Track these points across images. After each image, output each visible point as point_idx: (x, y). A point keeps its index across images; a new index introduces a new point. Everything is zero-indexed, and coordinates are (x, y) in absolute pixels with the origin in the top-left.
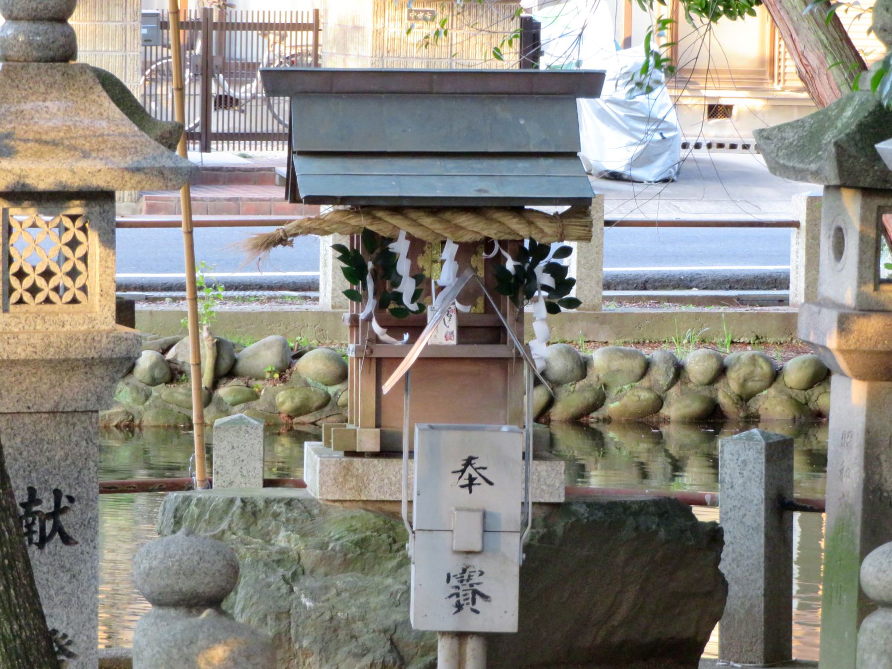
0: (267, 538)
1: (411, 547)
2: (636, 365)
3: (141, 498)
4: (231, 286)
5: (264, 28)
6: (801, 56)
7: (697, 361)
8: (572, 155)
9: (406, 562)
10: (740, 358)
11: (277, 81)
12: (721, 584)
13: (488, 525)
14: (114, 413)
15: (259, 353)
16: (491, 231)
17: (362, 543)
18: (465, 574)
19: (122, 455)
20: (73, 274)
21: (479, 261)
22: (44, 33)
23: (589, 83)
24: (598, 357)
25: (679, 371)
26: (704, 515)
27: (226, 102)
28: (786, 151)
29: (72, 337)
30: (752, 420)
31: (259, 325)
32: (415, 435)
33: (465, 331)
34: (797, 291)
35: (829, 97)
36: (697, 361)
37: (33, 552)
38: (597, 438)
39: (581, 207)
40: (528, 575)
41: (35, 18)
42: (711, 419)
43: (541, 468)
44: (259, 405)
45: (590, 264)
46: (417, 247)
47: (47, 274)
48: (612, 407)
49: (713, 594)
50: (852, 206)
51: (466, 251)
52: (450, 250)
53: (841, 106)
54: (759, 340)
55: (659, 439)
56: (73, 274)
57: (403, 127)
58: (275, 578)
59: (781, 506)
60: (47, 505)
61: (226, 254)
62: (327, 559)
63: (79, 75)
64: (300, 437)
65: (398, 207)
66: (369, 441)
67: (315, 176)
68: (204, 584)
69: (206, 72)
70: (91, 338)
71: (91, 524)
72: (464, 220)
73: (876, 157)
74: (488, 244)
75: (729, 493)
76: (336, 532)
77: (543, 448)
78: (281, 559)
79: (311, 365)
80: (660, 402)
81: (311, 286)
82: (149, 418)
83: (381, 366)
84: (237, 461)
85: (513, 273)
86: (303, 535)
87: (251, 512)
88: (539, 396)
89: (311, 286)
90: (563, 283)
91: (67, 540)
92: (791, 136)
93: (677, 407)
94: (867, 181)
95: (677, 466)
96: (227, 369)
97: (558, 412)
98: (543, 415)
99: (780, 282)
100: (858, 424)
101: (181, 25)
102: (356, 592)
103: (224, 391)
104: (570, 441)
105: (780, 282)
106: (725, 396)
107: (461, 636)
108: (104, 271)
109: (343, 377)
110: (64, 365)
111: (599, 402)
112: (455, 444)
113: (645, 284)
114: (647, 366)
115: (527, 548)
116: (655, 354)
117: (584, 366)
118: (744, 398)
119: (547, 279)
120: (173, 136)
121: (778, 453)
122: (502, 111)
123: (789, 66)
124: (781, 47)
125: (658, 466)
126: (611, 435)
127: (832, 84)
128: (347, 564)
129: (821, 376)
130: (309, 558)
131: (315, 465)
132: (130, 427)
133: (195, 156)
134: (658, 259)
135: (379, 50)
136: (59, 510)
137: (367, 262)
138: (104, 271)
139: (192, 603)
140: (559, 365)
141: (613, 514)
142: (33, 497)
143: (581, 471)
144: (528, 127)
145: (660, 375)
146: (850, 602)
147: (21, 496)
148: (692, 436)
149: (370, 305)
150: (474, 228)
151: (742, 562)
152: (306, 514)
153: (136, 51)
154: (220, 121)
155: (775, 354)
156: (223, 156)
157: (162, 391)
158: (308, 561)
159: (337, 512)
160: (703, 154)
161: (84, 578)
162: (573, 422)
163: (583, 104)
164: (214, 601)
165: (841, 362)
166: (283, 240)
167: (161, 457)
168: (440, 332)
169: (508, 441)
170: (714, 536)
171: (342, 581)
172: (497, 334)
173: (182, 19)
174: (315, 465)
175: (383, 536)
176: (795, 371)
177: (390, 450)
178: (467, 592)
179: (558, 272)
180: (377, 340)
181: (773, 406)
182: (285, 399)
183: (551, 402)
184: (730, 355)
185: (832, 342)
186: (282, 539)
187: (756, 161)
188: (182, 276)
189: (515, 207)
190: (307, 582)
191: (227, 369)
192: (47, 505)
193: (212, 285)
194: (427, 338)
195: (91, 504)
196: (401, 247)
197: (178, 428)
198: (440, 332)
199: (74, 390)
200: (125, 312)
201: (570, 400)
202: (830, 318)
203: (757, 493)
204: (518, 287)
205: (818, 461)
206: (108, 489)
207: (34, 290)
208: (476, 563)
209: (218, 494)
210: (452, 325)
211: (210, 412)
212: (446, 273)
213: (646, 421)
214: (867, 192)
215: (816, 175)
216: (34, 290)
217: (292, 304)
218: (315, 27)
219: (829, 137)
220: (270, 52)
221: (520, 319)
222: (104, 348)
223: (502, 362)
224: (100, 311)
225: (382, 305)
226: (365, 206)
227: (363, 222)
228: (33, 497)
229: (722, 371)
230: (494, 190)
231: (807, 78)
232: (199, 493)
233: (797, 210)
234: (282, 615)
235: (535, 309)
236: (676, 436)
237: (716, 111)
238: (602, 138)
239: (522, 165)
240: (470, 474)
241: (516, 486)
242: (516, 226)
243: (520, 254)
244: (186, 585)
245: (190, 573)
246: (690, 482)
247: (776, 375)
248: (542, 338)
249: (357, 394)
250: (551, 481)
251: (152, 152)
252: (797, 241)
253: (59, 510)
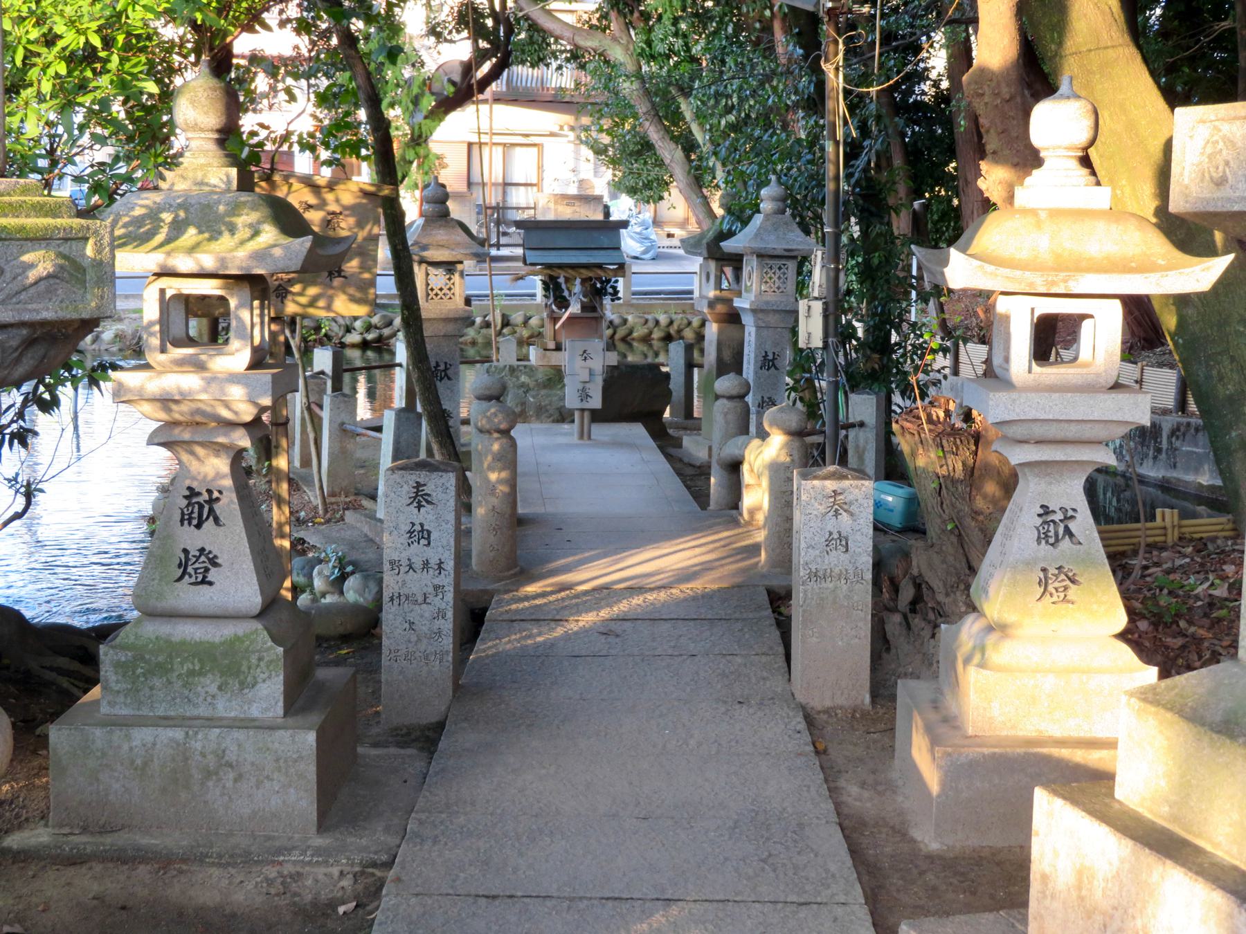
0: (518, 378)
1: (566, 381)
2: (643, 321)
3: (478, 365)
4: (507, 295)
5: (518, 208)
6: (697, 216)
7: (663, 319)
8: (618, 249)
9: (564, 386)
10: (678, 318)
11: (519, 224)
12: (670, 392)
13: (591, 373)
14: (468, 338)
15: (517, 318)
16: (590, 274)
17: (549, 380)
18: (584, 389)
19: (471, 352)
20: (450, 289)
21: (587, 285)
22: (438, 207)
23: (624, 224)
24: (630, 318)
25: (657, 322)
26: (664, 369)
27: (505, 234)
28: (691, 245)
29: (450, 310)
30: (682, 338)
31: (516, 308)
32: (567, 343)
33: (584, 308)
34: (696, 294)
35: (705, 228)
36: (663, 319)
37: (438, 383)
38: (630, 345)
39: (621, 268)
40: (606, 390)
41: (436, 202)
42: (668, 338)
43: (609, 354)
44: (517, 335)
45: (627, 286)
46: (567, 280)
47: (441, 289)
48: (635, 335)
49: (666, 397)
50: (712, 265)
51: (584, 281)
52: (578, 281)
53: (709, 231)
54: (684, 312)
55: (651, 346)
56: (450, 289)
57: (561, 240)
58: (521, 391)
59: (690, 366)
60: (442, 367)
61: (503, 285)
62: (538, 385)
63: (61, 44)
64: (529, 344)
65: (561, 266)
66: (552, 345)
67: (533, 256)
68: (494, 392)
69: (498, 223)
70: (457, 310)
71: (457, 373)
72: (583, 271)
73: (720, 248)
74: (591, 279)
75: (672, 362)
76: (540, 376)
77: (611, 346)
78: (523, 385)
79: (534, 322)
80: (651, 333)
81: (534, 295)
82: (480, 340)
83: (555, 320)
84: (507, 353)
85: (598, 289)
86: (530, 377)
87: (513, 370)
88: (609, 332)
89: (534, 295)
90: (616, 292)
91: (449, 379)
92: (692, 241)
93: (657, 334)
94: (718, 256)
95: (657, 355)
96: (506, 323)
97: (617, 336)
98: (612, 337)
99: (691, 292)
100: (715, 337)
101: (487, 208)
102: (548, 396)
103: (505, 331)
104: (621, 346)
105: (691, 292)
106: (672, 331)
107: (583, 410)
108: (460, 287)
109: (543, 326)
110: (447, 320)
111: (631, 333)
112: (580, 346)
113: (646, 293)
114: (646, 321)
115: (605, 381)
116: (649, 317)
117: (625, 321)
118: (679, 331)
119: (610, 290)
120: (482, 243)
121: (689, 349)
122: (595, 234)
123: (693, 220)
124: (691, 214)
125: (650, 354)
126: (635, 344)
127: (707, 224)
128: (545, 387)
129: (703, 324)
130: (532, 384)
131: (533, 353)
132: (474, 343)
133: (494, 252)
134: (650, 285)
135: (556, 214)
136: (446, 369)
137: (552, 286)
138: (460, 287)
139: (489, 398)
140: (617, 321)
141: (634, 368)
142: (438, 365)
143: (625, 356)
144: (605, 241)
145: (651, 324)
146: (712, 397)
147: (433, 364)
148: (660, 344)
149: (552, 300)
150: (586, 273)
151: (677, 384)
152: (531, 370)
153: (474, 216)
154: (503, 240)
155: (689, 317)
156: (504, 252)
157: (484, 331)
158: (531, 386)
159: (541, 369)
160: (666, 250)
161: (455, 395)
162: (619, 340)
163: (623, 231)
164: (498, 398)
165: (709, 317)
166: (522, 278)
167: (484, 353)
168: (575, 308)
169: (597, 345)
170: (667, 375)
171: (543, 392)
172: (594, 309)
173: (801, 345)
174: (533, 353)
175: (556, 377)
176: (696, 322)
177: (558, 348)
178: (585, 395)
179: (614, 288)
180: (553, 311)
181: (689, 334)
182: (525, 333)
183: (614, 333)
184: (674, 317)
185: (706, 310)
186: (523, 378)
187: (681, 252)
188: (488, 292)
189: (600, 266)
190: (532, 393)
191: (506, 323)
192: (442, 367)
193: (501, 295)
194: (570, 310)
195: (457, 367)
196: (561, 280)
197: (488, 344)
198: (575, 308)
199: (450, 328)
200: (468, 301)
201: (621, 332)
202: (705, 303)
203: (682, 362)
204: (600, 293)
205: (702, 351)
206: (462, 363)
207: (437, 295)
208: (588, 385)
209: (501, 364)
210: (579, 306)
211: (501, 339)
212: (577, 288)
213: (646, 339)
214: (717, 260)
215: (700, 254)
216: (437, 295)
217: (528, 301)
218: (534, 208)
219: (705, 241)
220: (520, 216)
221: (601, 304)
222: (461, 314)
223: (596, 319)
224: (459, 302)
225: (555, 300)
226: (549, 266)
227: (549, 272)
228: (438, 365)
229: (671, 323)
230: (592, 260)
231: (699, 223)
232: (495, 363)
233: (696, 268)
234: (523, 404)
235: (607, 301)
236: (656, 344)
237: (670, 236)
238: (630, 243)
239: (602, 252)
240: (585, 356)
241: (600, 360)
242: (600, 272)
243: (602, 282)
244: (487, 393)
245: (489, 389)
246: (661, 359)
247: (689, 323)
248: (609, 310)
249: (548, 331)
250: (613, 359)
251: (477, 249)
252: (696, 279)
253: (446, 369)
